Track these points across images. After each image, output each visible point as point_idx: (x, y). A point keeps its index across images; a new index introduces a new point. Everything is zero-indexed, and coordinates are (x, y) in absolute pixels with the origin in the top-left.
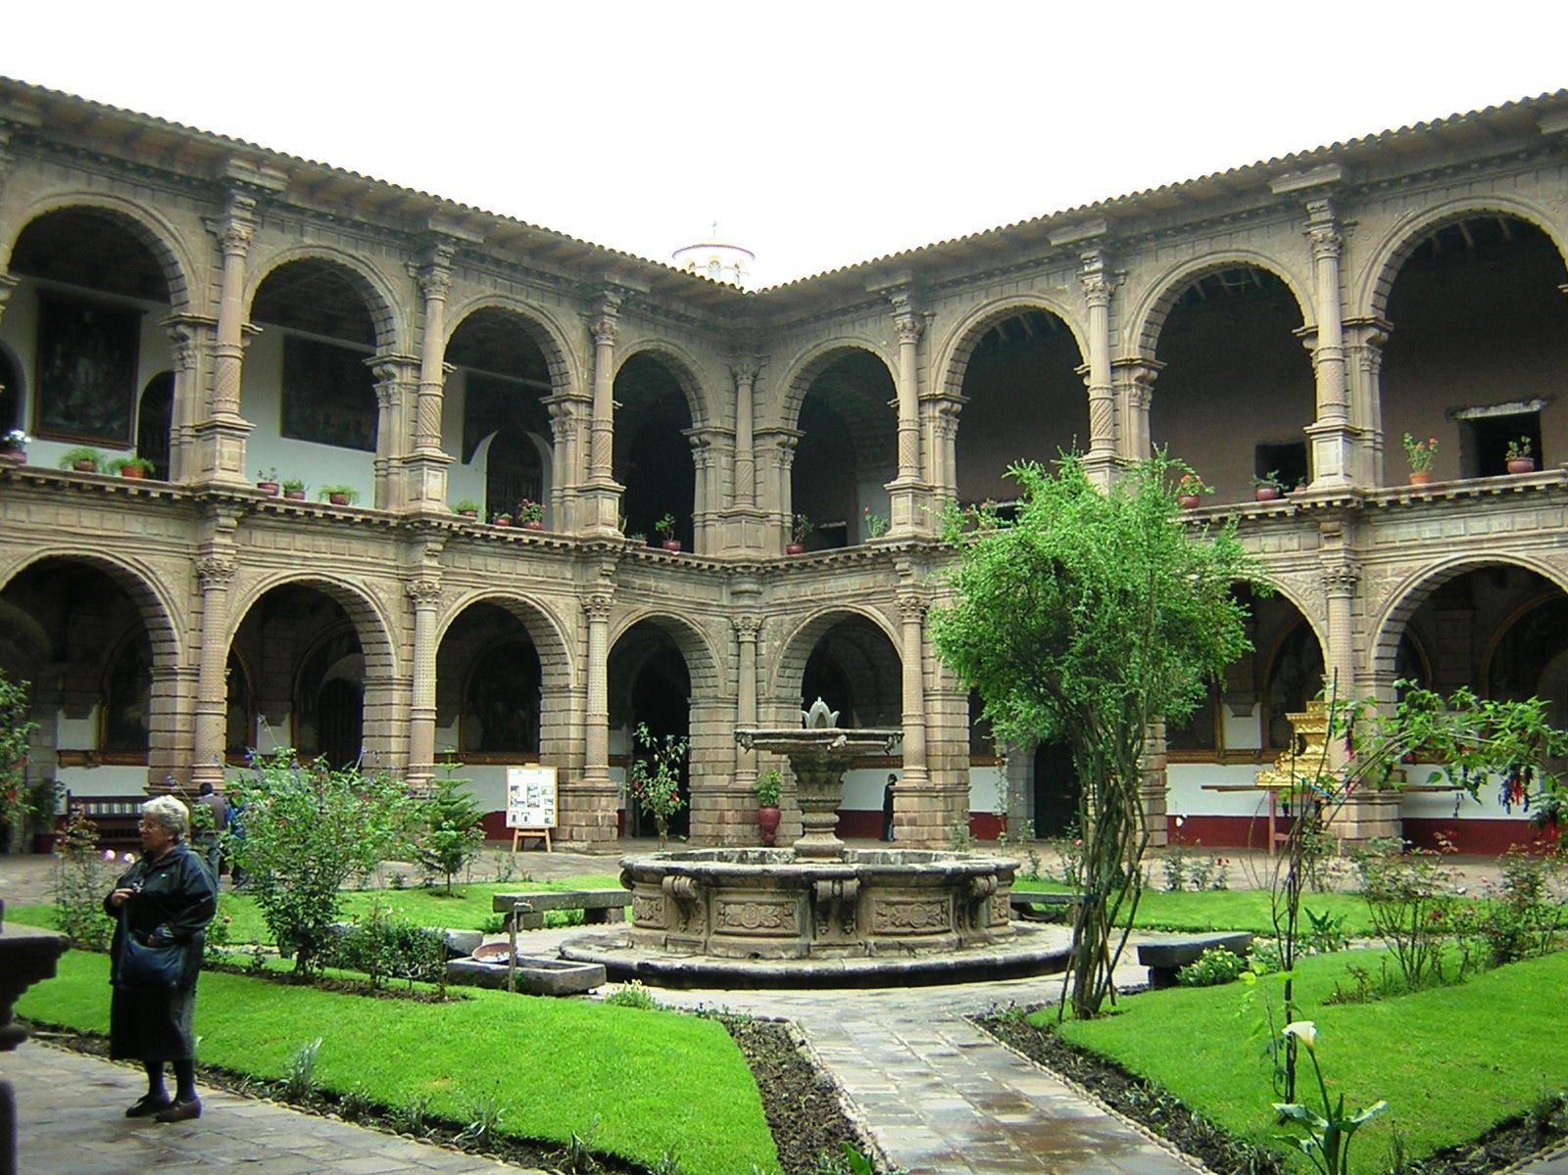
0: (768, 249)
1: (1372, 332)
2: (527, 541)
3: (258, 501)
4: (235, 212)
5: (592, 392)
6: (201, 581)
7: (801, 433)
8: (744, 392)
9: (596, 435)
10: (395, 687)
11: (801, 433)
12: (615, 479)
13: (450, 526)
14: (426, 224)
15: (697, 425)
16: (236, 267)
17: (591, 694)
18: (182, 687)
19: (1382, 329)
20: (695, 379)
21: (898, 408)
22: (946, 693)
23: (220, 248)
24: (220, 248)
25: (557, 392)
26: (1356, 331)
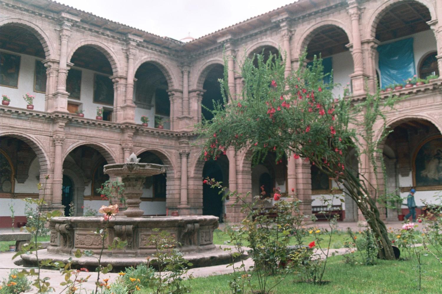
0: (186, 29)
1: (372, 44)
2: (14, 111)
3: (73, 118)
7: (205, 91)
8: (186, 77)
9: (127, 88)
10: (48, 172)
11: (205, 91)
12: (67, 91)
13: (68, 117)
14: (128, 36)
17: (55, 173)
19: (375, 43)
20: (168, 72)
22: (195, 178)
25: (170, 88)
26: (367, 44)
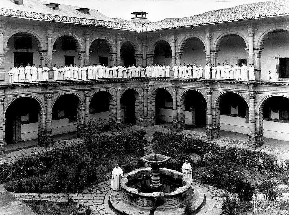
4: (49, 31)
5: (117, 52)
6: (46, 99)
15: (136, 53)
16: (50, 41)
18: (44, 117)
21: (172, 53)
23: (47, 37)
24: (47, 37)
